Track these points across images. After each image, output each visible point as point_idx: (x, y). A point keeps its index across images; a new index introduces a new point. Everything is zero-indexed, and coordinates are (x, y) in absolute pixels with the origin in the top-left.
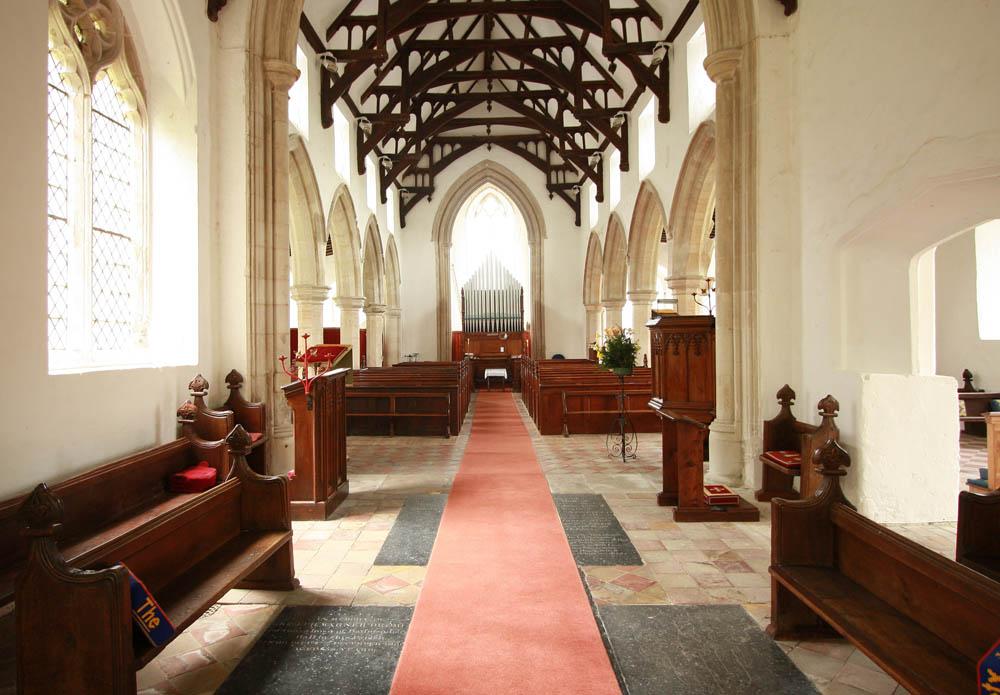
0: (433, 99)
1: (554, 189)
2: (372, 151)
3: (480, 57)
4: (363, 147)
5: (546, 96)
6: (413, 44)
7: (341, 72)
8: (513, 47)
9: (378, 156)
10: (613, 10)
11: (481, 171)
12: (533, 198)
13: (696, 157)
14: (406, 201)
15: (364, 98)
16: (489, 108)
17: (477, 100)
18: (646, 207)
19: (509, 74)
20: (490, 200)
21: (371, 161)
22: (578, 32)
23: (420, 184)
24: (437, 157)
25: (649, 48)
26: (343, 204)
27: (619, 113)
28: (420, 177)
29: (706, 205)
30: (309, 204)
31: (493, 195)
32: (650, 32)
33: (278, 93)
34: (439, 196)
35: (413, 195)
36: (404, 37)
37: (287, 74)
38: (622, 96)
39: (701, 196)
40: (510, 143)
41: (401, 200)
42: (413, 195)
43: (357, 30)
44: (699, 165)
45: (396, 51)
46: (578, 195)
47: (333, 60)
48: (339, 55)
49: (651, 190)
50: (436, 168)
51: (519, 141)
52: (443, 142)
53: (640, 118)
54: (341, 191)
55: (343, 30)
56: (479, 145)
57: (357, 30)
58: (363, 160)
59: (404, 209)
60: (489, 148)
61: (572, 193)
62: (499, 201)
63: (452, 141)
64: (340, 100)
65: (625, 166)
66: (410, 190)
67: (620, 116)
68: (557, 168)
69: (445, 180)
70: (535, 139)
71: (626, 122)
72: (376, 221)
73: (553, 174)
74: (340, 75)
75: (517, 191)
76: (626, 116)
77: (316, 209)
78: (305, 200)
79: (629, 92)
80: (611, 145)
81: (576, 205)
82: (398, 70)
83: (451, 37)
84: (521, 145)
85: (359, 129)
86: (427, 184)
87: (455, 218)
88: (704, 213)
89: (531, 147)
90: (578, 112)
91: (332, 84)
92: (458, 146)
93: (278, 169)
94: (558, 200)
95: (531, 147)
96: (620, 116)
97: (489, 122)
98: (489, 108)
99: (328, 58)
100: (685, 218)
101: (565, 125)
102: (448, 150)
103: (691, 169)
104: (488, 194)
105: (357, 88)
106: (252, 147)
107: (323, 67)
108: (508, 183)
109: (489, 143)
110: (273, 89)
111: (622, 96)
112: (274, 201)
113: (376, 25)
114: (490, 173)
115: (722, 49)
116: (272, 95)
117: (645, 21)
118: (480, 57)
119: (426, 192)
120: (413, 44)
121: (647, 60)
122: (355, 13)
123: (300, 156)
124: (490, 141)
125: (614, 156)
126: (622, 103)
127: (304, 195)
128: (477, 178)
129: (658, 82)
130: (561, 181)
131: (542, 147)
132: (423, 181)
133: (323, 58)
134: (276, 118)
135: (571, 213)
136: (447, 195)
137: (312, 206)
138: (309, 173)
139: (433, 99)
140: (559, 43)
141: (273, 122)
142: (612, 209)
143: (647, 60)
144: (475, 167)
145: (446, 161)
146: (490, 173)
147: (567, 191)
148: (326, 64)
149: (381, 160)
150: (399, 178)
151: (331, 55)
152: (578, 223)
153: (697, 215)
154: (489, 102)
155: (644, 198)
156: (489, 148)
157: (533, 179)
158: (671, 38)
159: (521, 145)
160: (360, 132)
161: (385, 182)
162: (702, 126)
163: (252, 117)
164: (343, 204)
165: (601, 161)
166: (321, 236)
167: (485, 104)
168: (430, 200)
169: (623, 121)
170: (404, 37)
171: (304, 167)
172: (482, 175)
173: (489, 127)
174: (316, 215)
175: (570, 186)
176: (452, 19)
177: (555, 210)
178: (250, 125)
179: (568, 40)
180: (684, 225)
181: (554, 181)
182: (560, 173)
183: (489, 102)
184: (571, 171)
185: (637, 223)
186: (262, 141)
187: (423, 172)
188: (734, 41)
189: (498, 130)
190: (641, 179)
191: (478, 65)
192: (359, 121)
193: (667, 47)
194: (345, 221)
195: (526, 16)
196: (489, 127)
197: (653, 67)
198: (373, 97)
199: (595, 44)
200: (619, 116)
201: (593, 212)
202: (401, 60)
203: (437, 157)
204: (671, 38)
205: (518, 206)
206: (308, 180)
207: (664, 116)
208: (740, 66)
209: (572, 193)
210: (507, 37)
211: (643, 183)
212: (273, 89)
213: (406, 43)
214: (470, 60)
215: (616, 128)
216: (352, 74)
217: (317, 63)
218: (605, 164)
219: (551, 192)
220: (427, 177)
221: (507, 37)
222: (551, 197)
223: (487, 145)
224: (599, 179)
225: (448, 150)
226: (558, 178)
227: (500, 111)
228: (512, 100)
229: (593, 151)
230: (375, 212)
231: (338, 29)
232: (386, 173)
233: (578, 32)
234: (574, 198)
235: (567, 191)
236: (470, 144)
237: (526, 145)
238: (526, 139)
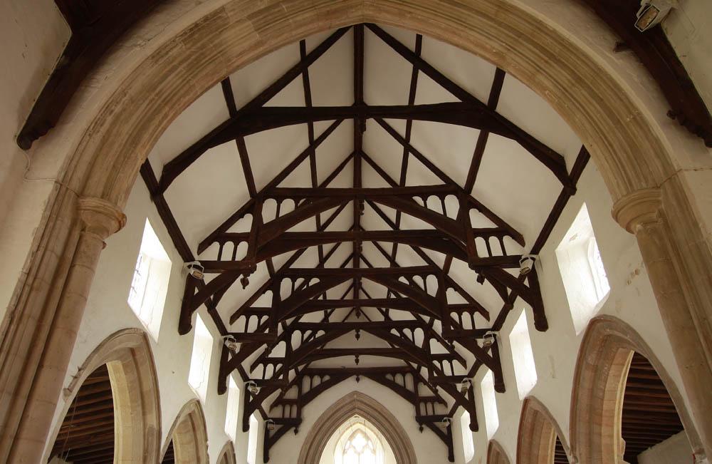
0: (303, 327)
1: (425, 421)
2: (236, 370)
3: (348, 210)
4: (226, 365)
5: (412, 325)
6: (287, 271)
7: (237, 351)
8: (384, 277)
9: (264, 419)
10: (450, 305)
11: (350, 402)
12: (403, 431)
13: (591, 359)
14: (272, 433)
15: (234, 318)
16: (358, 336)
17: (342, 328)
18: (532, 430)
19: (378, 303)
20: (359, 436)
21: (233, 383)
22: (427, 319)
23: (287, 415)
24: (306, 388)
25: (481, 333)
26: (193, 424)
27: (445, 418)
28: (288, 409)
29: (613, 417)
30: (144, 414)
31: (362, 432)
32: (481, 323)
33: (88, 236)
34: (306, 427)
35: (280, 426)
36: (289, 322)
37: (106, 215)
38: (488, 319)
39: (605, 407)
40: (378, 375)
41: (267, 431)
42: (280, 426)
43: (270, 367)
44: (596, 370)
45: (249, 198)
46: (449, 428)
47: (200, 269)
48: (238, 337)
49: (538, 408)
50: (304, 399)
51: (387, 373)
52: (312, 373)
53: (482, 383)
54: (193, 407)
55: (261, 366)
56: (351, 376)
57: (254, 319)
58: (248, 419)
59: (269, 442)
60: (358, 380)
61: (442, 425)
62: (368, 438)
63: (321, 372)
64: (235, 372)
65: (500, 386)
66: (276, 421)
67: (490, 336)
68: (426, 400)
69: (313, 412)
70: (403, 371)
71: (496, 342)
72: (233, 450)
73: (422, 406)
74: (237, 352)
75: (387, 425)
76: (495, 336)
77: (152, 420)
78: (140, 409)
79: (495, 311)
80: (461, 408)
81: (448, 438)
82: (269, 294)
83: (326, 312)
84: (389, 377)
85: (225, 347)
86: (294, 415)
87: (322, 452)
88: (612, 426)
89: (399, 379)
90: (446, 339)
91: (197, 291)
92: (327, 378)
93: (60, 322)
94: (429, 435)
95: (399, 379)
96: (490, 336)
97: (357, 353)
98: (358, 336)
99: (230, 339)
100: (590, 434)
101: (432, 353)
102: (317, 381)
103: (587, 375)
104: (359, 429)
105: (265, 404)
106: (27, 289)
107: (225, 347)
108: (376, 414)
109: (358, 375)
110: (83, 230)
111: (488, 319)
112: (40, 366)
113: (269, 316)
114: (358, 404)
115: (633, 191)
116: (81, 237)
117: (455, 362)
118: (348, 210)
119: (293, 424)
120: (297, 326)
121: (514, 272)
122: (254, 305)
123: (141, 356)
124: (358, 373)
125: (487, 378)
126: (491, 324)
127: (140, 402)
128: (346, 409)
129: (493, 359)
130: (430, 413)
131: (409, 378)
132: (290, 412)
133: (189, 267)
134: (78, 262)
135: (441, 447)
136: (314, 428)
137: (148, 417)
138: (151, 377)
139: (303, 327)
140: (423, 272)
141: (72, 266)
142: (490, 437)
143: (481, 342)
144: (343, 399)
145: (315, 392)
146: (358, 404)
147: (438, 424)
148: (228, 344)
149: (247, 385)
150: (246, 364)
151: (253, 382)
152: (451, 458)
153: (604, 430)
154: (357, 331)
155: (529, 419)
156: (358, 380)
157: (403, 411)
158: (536, 249)
159: (389, 377)
160: (225, 350)
161: (249, 406)
162: (593, 323)
163: (40, 253)
164: (193, 424)
165: (472, 387)
166: (154, 454)
167: (353, 332)
168: (296, 432)
169: (492, 340)
170: (289, 322)
171: (145, 368)
172: (350, 407)
173: (357, 357)
174: (152, 428)
175: (440, 418)
176: (329, 311)
177: (425, 444)
178: (33, 262)
179: (431, 268)
180: (590, 444)
181: (423, 413)
182: (493, 240)
183: (357, 331)
184: (440, 403)
185: (524, 450)
186: (46, 288)
187: (291, 402)
188: (647, 182)
189: (368, 361)
190: (522, 397)
191: (342, 223)
192: (225, 339)
193: (470, 381)
194: (193, 444)
195: (384, 309)
196: (357, 357)
197: (522, 277)
198: (243, 318)
199: (438, 326)
200: (464, 382)
201: (467, 442)
202: (287, 337)
203: (306, 388)
204: (536, 249)
205: (387, 439)
206: (147, 385)
207: (541, 323)
208: (663, 206)
209: (442, 425)
210: (367, 298)
211: (491, 444)
212: (83, 230)
213: (279, 271)
214: (337, 207)
215: (486, 348)
216: (245, 353)
217: (183, 271)
218: (476, 391)
219: (421, 424)
220: (295, 409)
221: (367, 298)
222: (421, 429)
223: (355, 377)
224: (471, 406)
225: (317, 381)
226: (428, 410)
227: (368, 340)
228: (381, 330)
229: (484, 331)
230: (234, 439)
231: (210, 244)
232: (230, 357)
233: (427, 319)
234: (445, 431)
235: (438, 424)
236: (339, 376)
237: (394, 376)
238: (394, 371)
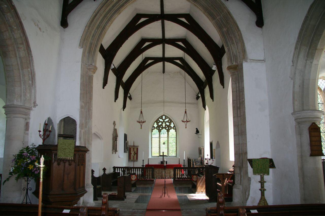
135: (254, 18)
